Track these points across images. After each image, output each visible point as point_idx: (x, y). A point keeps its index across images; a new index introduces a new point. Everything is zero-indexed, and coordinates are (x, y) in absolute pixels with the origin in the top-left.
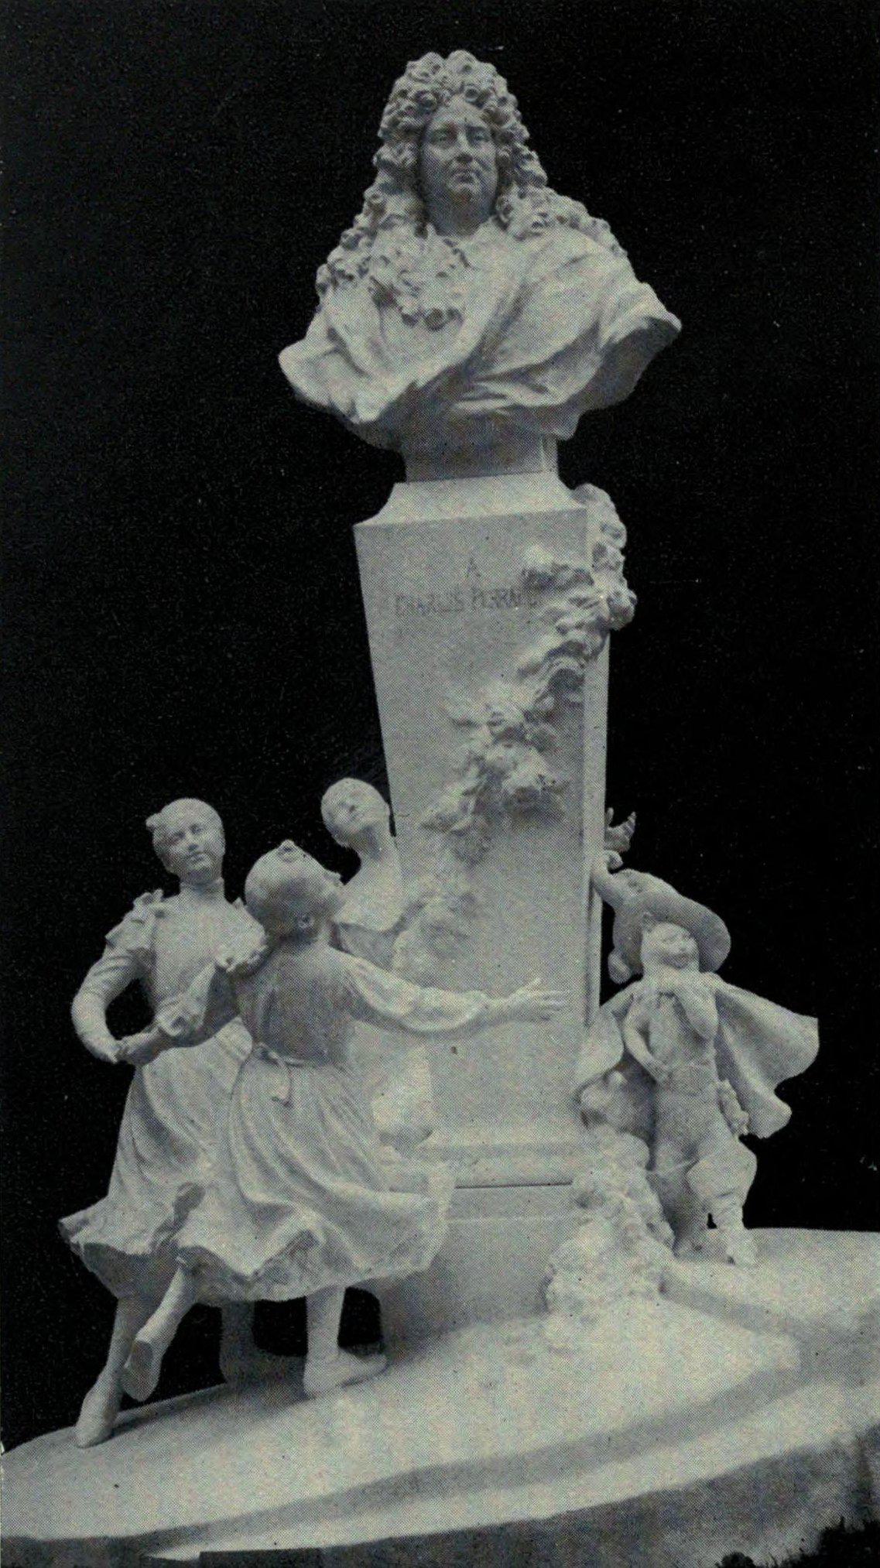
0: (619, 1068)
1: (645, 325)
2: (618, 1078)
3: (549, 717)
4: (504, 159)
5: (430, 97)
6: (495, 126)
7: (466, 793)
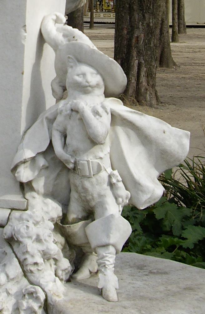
0: (44, 154)
2: (42, 162)
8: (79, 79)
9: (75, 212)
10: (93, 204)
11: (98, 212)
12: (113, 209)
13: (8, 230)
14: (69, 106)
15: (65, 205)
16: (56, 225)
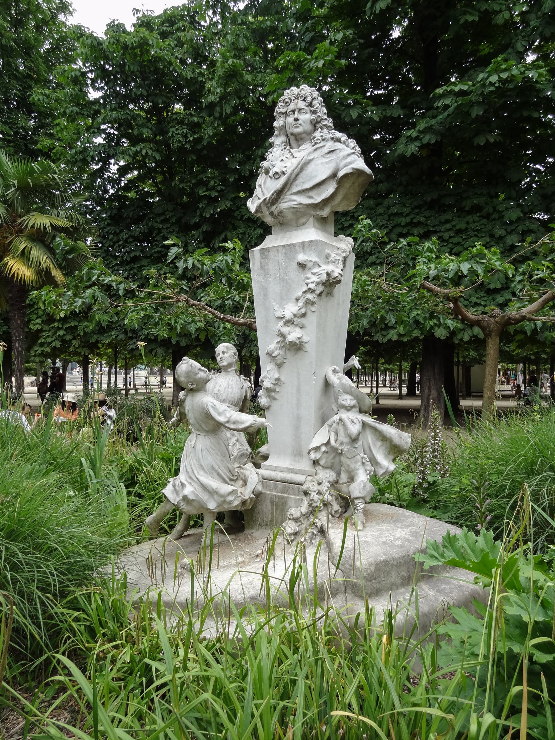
1: (351, 171)
3: (304, 315)
4: (314, 119)
5: (287, 100)
6: (311, 109)
7: (278, 342)
8: (344, 403)
9: (344, 477)
10: (352, 474)
11: (356, 478)
12: (362, 477)
13: (304, 487)
14: (338, 418)
15: (339, 474)
16: (332, 485)
